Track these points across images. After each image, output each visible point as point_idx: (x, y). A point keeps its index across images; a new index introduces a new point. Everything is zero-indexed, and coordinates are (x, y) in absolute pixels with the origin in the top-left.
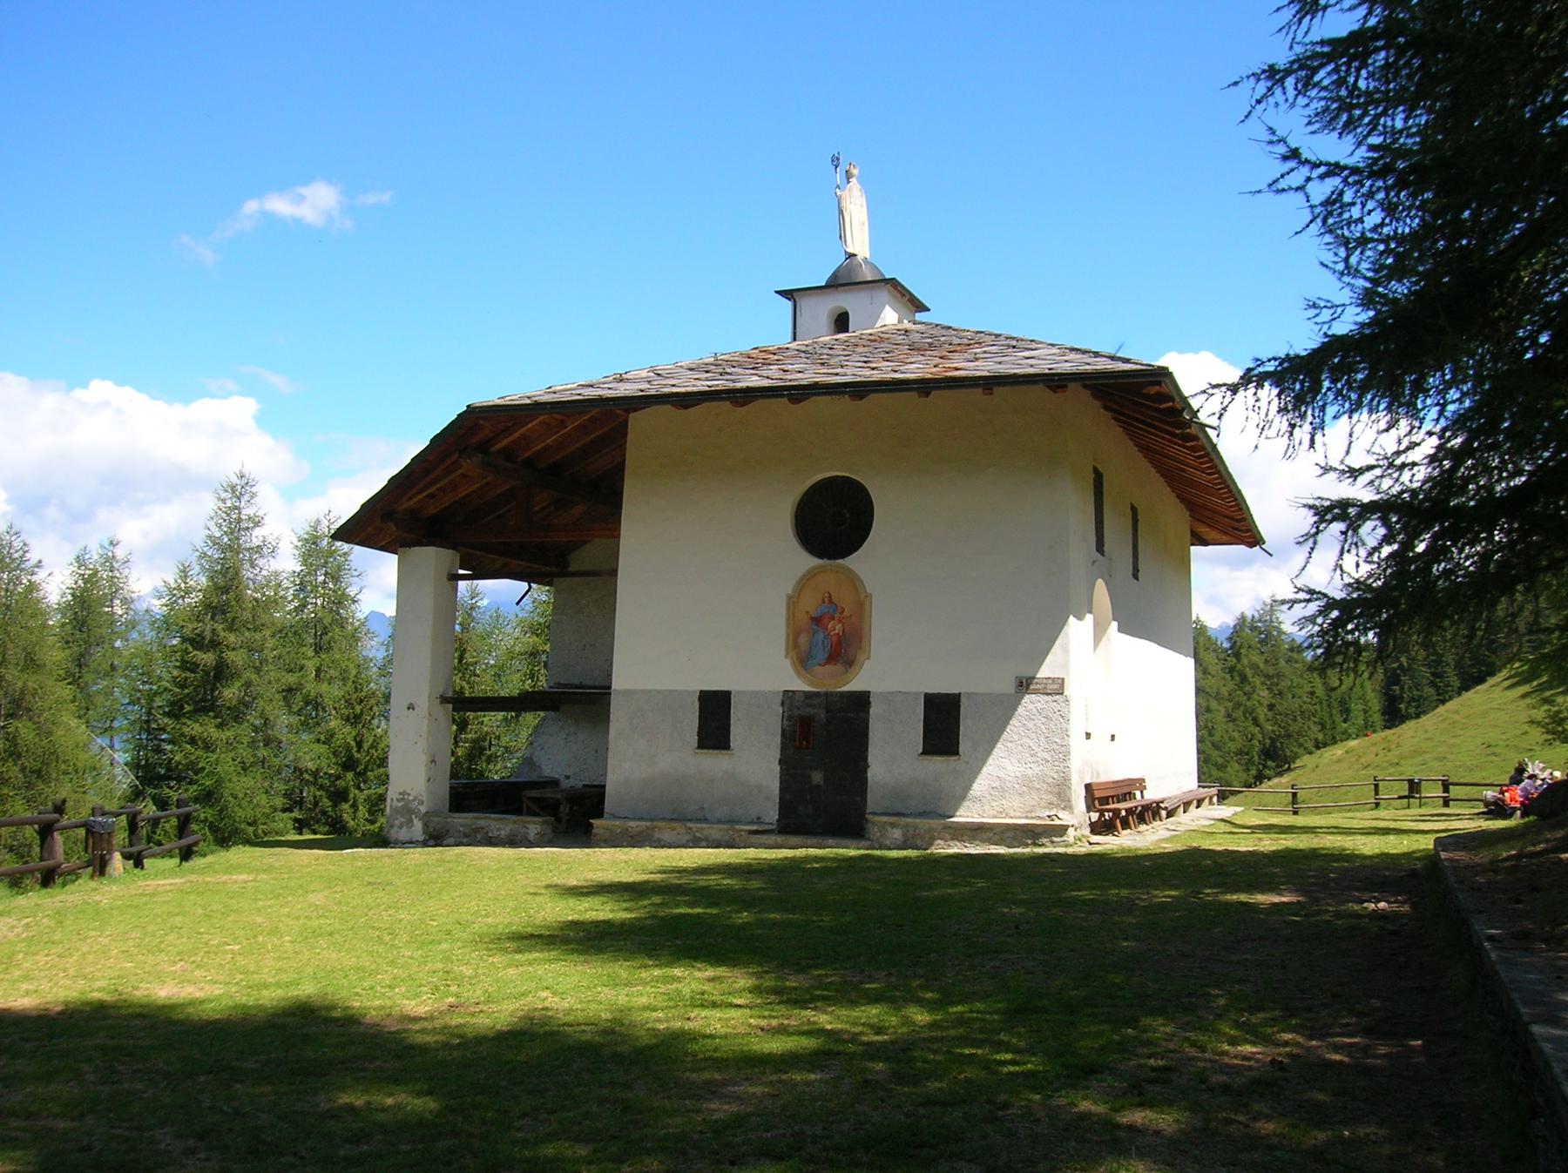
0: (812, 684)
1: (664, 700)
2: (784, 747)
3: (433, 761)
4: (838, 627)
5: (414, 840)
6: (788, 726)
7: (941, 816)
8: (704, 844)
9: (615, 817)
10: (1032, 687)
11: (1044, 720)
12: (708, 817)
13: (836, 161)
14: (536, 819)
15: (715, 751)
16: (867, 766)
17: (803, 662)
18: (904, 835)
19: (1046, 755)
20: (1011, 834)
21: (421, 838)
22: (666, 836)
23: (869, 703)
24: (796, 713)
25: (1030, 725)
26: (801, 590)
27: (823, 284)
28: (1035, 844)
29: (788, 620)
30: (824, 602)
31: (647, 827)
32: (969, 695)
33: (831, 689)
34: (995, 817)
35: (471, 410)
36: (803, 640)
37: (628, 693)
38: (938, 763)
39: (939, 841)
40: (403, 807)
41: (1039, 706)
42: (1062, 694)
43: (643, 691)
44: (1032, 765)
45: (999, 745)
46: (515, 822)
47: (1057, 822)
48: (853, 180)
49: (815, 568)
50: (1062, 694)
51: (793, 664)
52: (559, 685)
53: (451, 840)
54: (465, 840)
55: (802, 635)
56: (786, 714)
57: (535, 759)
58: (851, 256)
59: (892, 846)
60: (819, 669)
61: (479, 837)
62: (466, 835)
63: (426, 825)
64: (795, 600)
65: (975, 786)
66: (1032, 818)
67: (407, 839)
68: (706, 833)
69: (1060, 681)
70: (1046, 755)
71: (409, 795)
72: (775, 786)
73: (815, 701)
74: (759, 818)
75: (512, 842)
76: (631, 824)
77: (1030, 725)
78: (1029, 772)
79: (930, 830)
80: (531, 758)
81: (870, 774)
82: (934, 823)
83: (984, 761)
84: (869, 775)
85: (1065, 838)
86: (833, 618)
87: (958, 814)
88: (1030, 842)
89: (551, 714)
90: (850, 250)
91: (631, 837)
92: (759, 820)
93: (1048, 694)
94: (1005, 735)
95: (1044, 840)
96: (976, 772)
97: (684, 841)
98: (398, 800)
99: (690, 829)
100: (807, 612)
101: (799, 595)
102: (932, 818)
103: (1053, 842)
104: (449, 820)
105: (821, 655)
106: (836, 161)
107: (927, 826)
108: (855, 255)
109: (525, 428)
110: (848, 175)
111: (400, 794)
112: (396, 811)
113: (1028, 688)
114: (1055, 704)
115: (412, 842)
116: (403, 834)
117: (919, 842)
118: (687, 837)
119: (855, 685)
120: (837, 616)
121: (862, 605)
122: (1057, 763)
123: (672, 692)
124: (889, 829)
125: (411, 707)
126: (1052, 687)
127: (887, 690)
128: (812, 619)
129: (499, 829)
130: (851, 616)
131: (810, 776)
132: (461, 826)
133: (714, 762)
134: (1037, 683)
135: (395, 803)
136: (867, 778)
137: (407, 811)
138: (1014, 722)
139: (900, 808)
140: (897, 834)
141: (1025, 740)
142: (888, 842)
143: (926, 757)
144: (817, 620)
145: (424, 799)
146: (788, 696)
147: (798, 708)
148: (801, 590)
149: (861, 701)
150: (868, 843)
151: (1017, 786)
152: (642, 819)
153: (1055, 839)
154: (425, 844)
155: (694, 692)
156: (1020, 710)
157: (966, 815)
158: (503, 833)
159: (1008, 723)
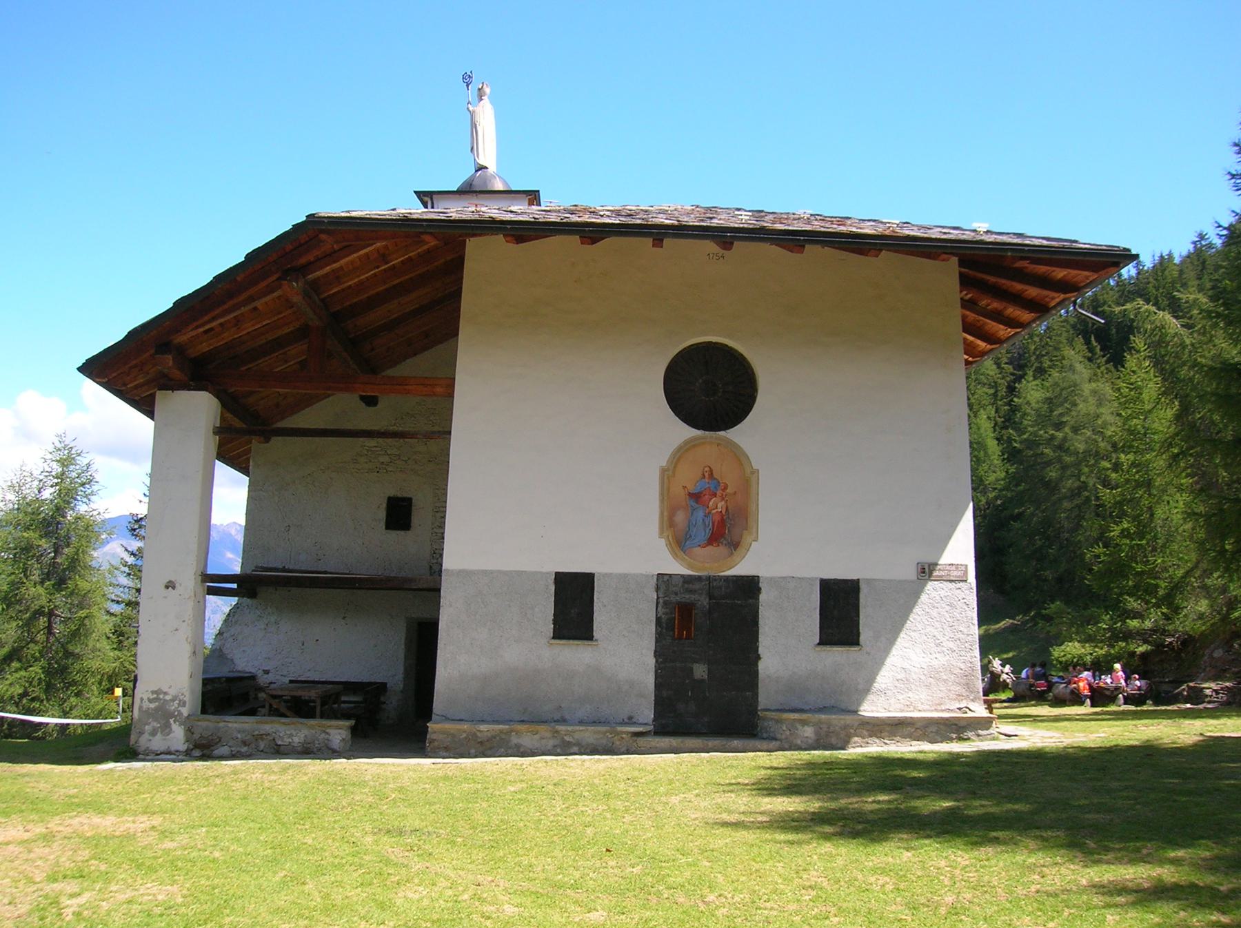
0: (690, 567)
1: (512, 582)
2: (659, 637)
3: (194, 652)
4: (721, 505)
5: (173, 749)
6: (665, 614)
7: (849, 711)
8: (575, 749)
9: (446, 719)
10: (935, 574)
11: (948, 608)
12: (567, 717)
13: (467, 79)
14: (341, 723)
15: (576, 642)
16: (758, 657)
17: (680, 543)
18: (817, 733)
19: (951, 645)
20: (934, 729)
21: (183, 747)
22: (527, 741)
23: (759, 590)
24: (673, 598)
25: (934, 613)
26: (679, 460)
27: (455, 189)
28: (960, 739)
29: (662, 494)
30: (704, 476)
31: (501, 731)
32: (868, 581)
33: (712, 574)
34: (902, 711)
35: (312, 220)
36: (680, 517)
37: (464, 574)
38: (837, 655)
39: (856, 739)
40: (156, 709)
41: (943, 593)
42: (966, 581)
43: (485, 572)
44: (938, 655)
45: (902, 635)
46: (312, 727)
47: (970, 714)
48: (485, 98)
49: (692, 440)
50: (966, 581)
51: (669, 545)
52: (258, 568)
53: (224, 750)
54: (244, 749)
55: (679, 513)
56: (661, 601)
57: (225, 651)
58: (481, 168)
59: (787, 747)
60: (698, 550)
61: (262, 745)
62: (244, 743)
63: (189, 731)
64: (670, 473)
65: (879, 679)
66: (943, 711)
67: (163, 749)
68: (577, 736)
69: (963, 568)
70: (951, 645)
71: (166, 693)
72: (650, 681)
73: (697, 586)
74: (630, 718)
75: (307, 752)
76: (483, 727)
77: (934, 613)
78: (935, 662)
79: (846, 727)
80: (221, 650)
81: (762, 666)
82: (848, 719)
83: (887, 651)
84: (760, 668)
85: (991, 731)
86: (715, 495)
87: (862, 708)
88: (954, 736)
89: (246, 601)
90: (482, 162)
91: (481, 743)
92: (630, 721)
93: (951, 581)
94: (908, 625)
95: (970, 734)
96: (879, 664)
97: (549, 747)
98: (150, 701)
99: (557, 732)
100: (684, 487)
101: (675, 467)
102: (831, 713)
103: (979, 735)
104: (221, 725)
105: (702, 534)
106: (467, 79)
107: (842, 722)
108: (486, 168)
109: (355, 255)
110: (481, 94)
111: (153, 692)
112: (146, 713)
113: (930, 575)
114: (959, 591)
115: (169, 753)
116: (158, 743)
117: (834, 741)
118: (551, 743)
119: (742, 568)
120: (719, 493)
121: (748, 482)
122: (963, 653)
123: (520, 573)
124: (799, 727)
125: (170, 585)
126: (955, 573)
127: (779, 575)
128: (691, 495)
129: (291, 736)
130: (735, 493)
131: (692, 669)
132: (239, 732)
133: (574, 654)
134: (940, 570)
135: (146, 705)
136: (757, 672)
137: (163, 714)
138: (917, 610)
139: (796, 703)
140: (808, 732)
141: (929, 629)
142: (799, 742)
143: (824, 648)
144: (696, 497)
145: (186, 699)
146: (663, 580)
147: (676, 594)
148: (679, 460)
149: (750, 586)
150: (778, 743)
151: (923, 677)
152: (497, 722)
153: (980, 732)
154: (188, 755)
155: (544, 575)
156: (924, 597)
157: (872, 708)
158: (296, 740)
159: (911, 611)
